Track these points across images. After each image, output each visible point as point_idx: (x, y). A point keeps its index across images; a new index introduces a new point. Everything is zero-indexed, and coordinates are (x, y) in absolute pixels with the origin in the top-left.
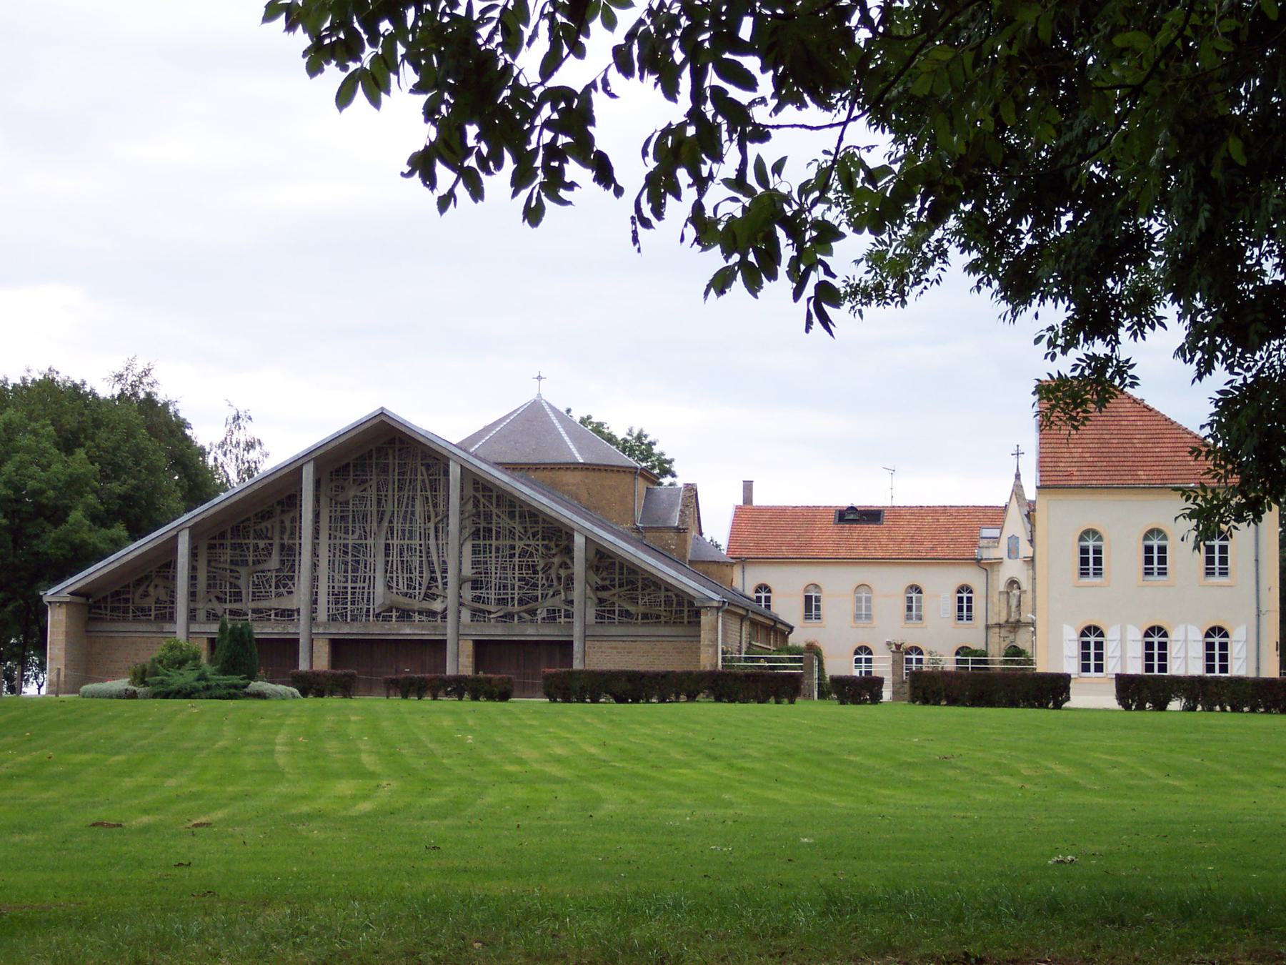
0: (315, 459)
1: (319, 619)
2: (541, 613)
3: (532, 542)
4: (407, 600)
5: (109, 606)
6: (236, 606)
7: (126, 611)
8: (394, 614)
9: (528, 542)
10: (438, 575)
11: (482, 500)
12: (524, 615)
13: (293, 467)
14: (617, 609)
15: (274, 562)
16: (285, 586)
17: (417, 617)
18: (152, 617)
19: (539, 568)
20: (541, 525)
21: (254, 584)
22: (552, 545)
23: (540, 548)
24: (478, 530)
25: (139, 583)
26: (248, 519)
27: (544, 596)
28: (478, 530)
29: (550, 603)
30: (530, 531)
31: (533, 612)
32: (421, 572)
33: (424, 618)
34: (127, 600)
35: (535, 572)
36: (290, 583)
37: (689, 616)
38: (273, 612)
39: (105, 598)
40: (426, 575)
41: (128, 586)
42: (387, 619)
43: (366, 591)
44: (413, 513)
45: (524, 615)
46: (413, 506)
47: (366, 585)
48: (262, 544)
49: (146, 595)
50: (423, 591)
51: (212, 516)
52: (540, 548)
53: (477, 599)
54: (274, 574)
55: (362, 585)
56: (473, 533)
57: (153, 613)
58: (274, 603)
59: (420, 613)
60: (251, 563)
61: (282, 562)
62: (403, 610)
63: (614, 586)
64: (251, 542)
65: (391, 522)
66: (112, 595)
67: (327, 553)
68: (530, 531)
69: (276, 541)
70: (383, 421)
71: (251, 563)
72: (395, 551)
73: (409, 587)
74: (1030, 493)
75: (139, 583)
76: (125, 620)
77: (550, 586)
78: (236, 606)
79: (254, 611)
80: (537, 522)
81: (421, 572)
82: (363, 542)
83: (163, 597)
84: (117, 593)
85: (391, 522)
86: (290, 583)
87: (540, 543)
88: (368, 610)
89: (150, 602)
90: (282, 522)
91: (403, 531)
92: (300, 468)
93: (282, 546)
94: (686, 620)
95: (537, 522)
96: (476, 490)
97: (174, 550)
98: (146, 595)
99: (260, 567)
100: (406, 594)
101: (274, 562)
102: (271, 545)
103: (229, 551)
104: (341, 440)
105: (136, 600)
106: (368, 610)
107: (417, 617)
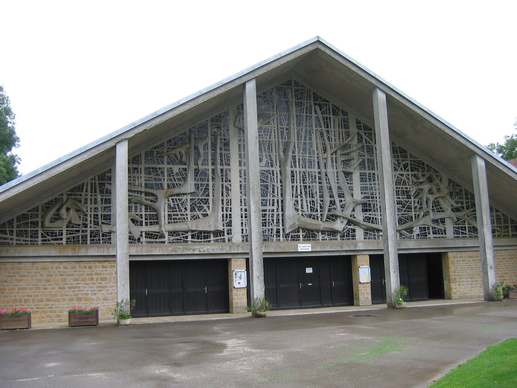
0: (130, 140)
1: (234, 240)
2: (417, 231)
3: (405, 173)
4: (309, 220)
5: (15, 229)
6: (154, 228)
7: (34, 235)
8: (301, 234)
9: (401, 173)
10: (337, 199)
11: (364, 137)
12: (404, 232)
13: (238, 83)
14: (467, 226)
15: (190, 186)
16: (200, 208)
17: (320, 236)
18: (64, 241)
19: (412, 194)
20: (409, 159)
21: (169, 207)
22: (420, 174)
23: (410, 177)
24: (364, 161)
25: (47, 207)
26: (162, 145)
27: (417, 217)
28: (364, 161)
29: (422, 222)
30: (402, 164)
31: (410, 230)
32: (321, 196)
33: (326, 237)
34: (35, 224)
35: (409, 197)
36: (205, 206)
37: (512, 232)
38: (189, 235)
39: (11, 222)
40: (327, 199)
41: (37, 209)
42: (296, 238)
43: (275, 213)
44: (311, 145)
45: (404, 232)
46: (310, 139)
47: (275, 208)
48: (176, 169)
49: (57, 217)
50: (326, 213)
51: (157, 127)
52: (410, 177)
53: (367, 219)
54: (189, 197)
55: (271, 208)
56: (360, 164)
57: (64, 237)
58: (192, 225)
59: (323, 232)
60: (165, 187)
61: (197, 187)
62: (309, 230)
63: (463, 208)
64: (166, 166)
65: (294, 152)
66: (19, 219)
67: (238, 179)
68: (402, 164)
69: (193, 167)
70: (317, 49)
71: (165, 187)
72: (298, 177)
73: (312, 209)
74: (385, 306)
75: (47, 207)
76: (33, 244)
77: (421, 208)
78: (154, 228)
79: (171, 233)
80: (406, 157)
81: (321, 196)
82: (270, 169)
83: (76, 221)
84: (24, 216)
85: (294, 152)
86: (205, 206)
87: (410, 173)
88: (278, 231)
89: (62, 226)
90: (196, 148)
91: (304, 160)
92: (244, 85)
93: (197, 171)
94: (510, 234)
95: (406, 157)
96: (359, 127)
97: (114, 158)
98: (57, 217)
99: (176, 191)
100: (310, 216)
101: (190, 186)
102: (185, 170)
103: (143, 175)
104: (200, 101)
105: (47, 223)
106: (278, 231)
107: (320, 236)
